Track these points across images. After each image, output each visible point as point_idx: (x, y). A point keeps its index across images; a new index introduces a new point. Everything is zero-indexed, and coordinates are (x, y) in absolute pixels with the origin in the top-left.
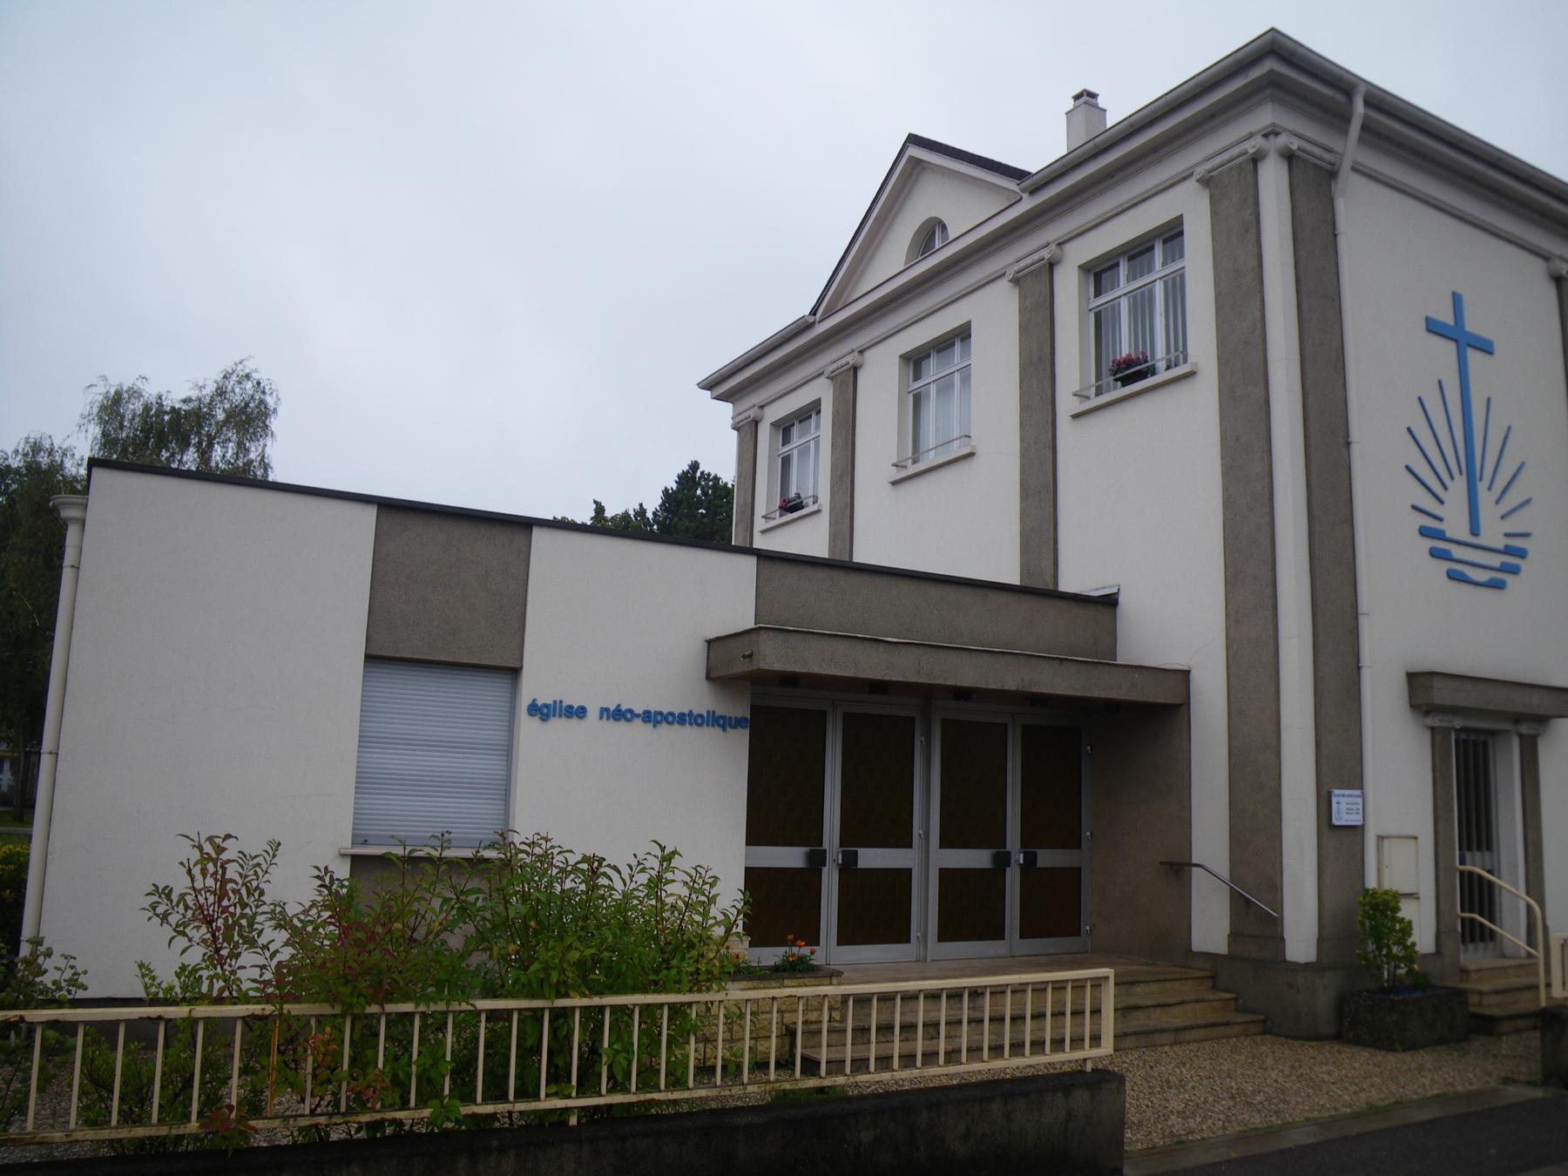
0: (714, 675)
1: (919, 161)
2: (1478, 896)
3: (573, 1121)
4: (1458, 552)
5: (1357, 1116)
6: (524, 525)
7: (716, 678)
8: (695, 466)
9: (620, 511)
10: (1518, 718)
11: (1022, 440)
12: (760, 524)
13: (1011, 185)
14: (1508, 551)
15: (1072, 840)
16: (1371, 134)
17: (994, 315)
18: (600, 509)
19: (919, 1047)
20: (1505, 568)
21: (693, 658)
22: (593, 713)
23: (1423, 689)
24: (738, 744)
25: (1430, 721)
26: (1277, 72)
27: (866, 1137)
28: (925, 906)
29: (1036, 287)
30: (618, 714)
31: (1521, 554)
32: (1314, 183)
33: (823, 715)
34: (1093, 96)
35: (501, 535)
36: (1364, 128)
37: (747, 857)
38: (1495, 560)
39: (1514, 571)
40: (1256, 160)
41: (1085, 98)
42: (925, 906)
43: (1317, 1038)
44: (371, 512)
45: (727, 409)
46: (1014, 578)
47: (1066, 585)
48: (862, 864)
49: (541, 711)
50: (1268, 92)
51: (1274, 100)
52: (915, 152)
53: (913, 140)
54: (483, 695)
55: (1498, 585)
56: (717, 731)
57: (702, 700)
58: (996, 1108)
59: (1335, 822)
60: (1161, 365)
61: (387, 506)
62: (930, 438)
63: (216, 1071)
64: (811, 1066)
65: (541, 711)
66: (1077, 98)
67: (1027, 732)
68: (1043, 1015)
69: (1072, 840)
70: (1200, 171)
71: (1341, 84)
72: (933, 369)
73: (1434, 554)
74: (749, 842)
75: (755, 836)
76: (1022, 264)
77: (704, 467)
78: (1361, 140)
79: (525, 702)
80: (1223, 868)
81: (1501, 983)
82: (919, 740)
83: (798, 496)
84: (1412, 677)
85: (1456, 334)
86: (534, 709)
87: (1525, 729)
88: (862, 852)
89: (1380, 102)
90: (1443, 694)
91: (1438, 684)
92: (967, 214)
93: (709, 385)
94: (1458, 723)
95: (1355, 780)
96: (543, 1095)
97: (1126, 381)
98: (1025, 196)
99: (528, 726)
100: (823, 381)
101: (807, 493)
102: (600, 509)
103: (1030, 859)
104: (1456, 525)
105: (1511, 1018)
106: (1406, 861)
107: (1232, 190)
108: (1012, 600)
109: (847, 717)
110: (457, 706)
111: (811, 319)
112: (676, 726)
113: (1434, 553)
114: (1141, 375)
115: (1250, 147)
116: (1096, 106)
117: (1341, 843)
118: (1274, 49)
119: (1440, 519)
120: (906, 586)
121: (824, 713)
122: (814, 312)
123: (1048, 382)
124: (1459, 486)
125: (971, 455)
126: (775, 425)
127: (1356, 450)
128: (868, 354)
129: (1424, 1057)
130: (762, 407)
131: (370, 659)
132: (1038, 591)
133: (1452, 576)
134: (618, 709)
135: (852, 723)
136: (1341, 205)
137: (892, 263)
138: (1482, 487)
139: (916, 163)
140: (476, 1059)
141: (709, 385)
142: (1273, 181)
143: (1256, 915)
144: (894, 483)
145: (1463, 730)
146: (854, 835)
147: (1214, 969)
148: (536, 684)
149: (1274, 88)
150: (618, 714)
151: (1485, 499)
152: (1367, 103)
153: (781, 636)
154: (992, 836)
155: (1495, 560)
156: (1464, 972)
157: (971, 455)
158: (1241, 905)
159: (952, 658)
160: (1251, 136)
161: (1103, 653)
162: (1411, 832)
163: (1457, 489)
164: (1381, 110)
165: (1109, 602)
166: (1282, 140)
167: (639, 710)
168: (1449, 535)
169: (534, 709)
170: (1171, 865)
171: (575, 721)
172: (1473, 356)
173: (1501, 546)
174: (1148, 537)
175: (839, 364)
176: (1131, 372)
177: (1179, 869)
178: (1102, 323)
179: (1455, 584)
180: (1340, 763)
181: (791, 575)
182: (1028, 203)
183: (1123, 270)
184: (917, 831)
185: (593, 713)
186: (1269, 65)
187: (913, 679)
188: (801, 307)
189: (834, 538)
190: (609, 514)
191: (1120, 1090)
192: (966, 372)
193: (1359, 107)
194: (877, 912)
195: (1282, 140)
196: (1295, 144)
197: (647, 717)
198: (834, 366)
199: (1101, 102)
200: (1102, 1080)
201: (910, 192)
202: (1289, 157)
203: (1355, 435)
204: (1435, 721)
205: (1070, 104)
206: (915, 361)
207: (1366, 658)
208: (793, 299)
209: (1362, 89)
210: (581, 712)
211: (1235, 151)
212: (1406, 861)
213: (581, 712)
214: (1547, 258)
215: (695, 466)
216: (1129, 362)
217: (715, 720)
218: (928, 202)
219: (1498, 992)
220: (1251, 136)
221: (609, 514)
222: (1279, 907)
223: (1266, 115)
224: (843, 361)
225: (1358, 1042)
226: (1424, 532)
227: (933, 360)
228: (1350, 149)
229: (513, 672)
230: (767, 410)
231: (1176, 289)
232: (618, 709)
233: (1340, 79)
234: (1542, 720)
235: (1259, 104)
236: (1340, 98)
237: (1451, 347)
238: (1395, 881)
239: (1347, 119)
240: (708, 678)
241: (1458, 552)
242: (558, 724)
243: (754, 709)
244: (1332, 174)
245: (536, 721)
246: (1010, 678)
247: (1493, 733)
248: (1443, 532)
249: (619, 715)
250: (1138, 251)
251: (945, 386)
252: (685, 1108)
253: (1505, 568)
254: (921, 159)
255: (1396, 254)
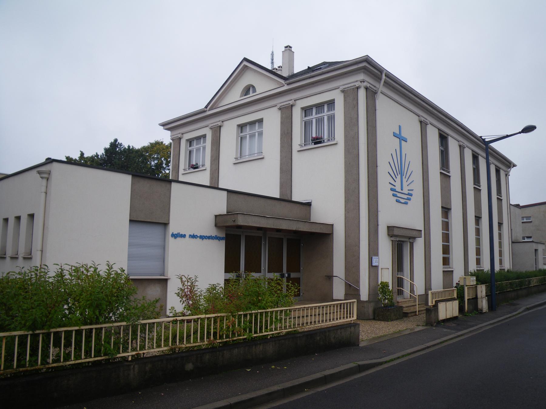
0: (219, 225)
1: (247, 66)
2: (400, 282)
3: (130, 359)
4: (399, 195)
5: (392, 334)
7: (217, 226)
8: (116, 140)
9: (90, 155)
10: (410, 238)
11: (281, 156)
12: (181, 171)
13: (282, 81)
15: (298, 271)
16: (386, 84)
17: (272, 119)
18: (82, 154)
19: (279, 325)
21: (211, 221)
22: (187, 236)
23: (390, 229)
24: (223, 243)
25: (392, 239)
26: (367, 66)
27: (318, 338)
29: (287, 112)
30: (193, 236)
31: (411, 195)
32: (371, 94)
34: (291, 47)
36: (385, 82)
37: (225, 276)
38: (406, 197)
39: (409, 199)
40: (358, 88)
41: (288, 48)
43: (370, 320)
45: (169, 132)
46: (278, 196)
47: (294, 199)
48: (291, 277)
49: (175, 236)
50: (363, 70)
51: (364, 73)
52: (245, 63)
53: (245, 59)
54: (157, 231)
55: (406, 203)
57: (213, 232)
58: (339, 331)
60: (326, 141)
62: (247, 151)
63: (209, 326)
64: (285, 327)
65: (175, 236)
66: (286, 47)
67: (288, 240)
68: (295, 318)
69: (298, 271)
71: (380, 70)
72: (248, 131)
73: (394, 195)
74: (225, 272)
75: (226, 271)
76: (282, 104)
77: (119, 141)
78: (384, 85)
80: (343, 276)
81: (407, 305)
82: (263, 242)
83: (197, 164)
84: (388, 227)
85: (399, 136)
87: (411, 241)
88: (291, 274)
89: (389, 76)
90: (396, 232)
91: (395, 229)
92: (264, 86)
93: (163, 125)
94: (398, 239)
95: (377, 254)
96: (147, 348)
97: (315, 143)
98: (286, 85)
99: (171, 242)
100: (208, 128)
101: (200, 163)
102: (82, 154)
103: (289, 275)
104: (398, 188)
105: (411, 313)
106: (386, 276)
107: (350, 95)
108: (276, 202)
109: (246, 236)
110: (151, 234)
111: (206, 109)
114: (320, 142)
115: (357, 84)
116: (291, 51)
117: (373, 269)
118: (367, 60)
120: (262, 200)
121: (240, 235)
122: (206, 107)
123: (290, 140)
124: (399, 177)
125: (263, 158)
126: (187, 140)
127: (378, 168)
128: (224, 123)
129: (395, 323)
130: (182, 134)
131: (131, 221)
132: (285, 199)
133: (397, 201)
134: (193, 235)
136: (378, 102)
137: (235, 97)
138: (404, 177)
139: (246, 66)
140: (38, 349)
141: (163, 125)
142: (362, 94)
143: (352, 290)
144: (234, 164)
145: (399, 241)
148: (173, 228)
149: (365, 70)
150: (193, 236)
151: (404, 180)
152: (385, 75)
153: (243, 216)
154: (279, 269)
156: (398, 302)
157: (263, 158)
158: (348, 286)
159: (281, 221)
160: (357, 81)
161: (307, 219)
163: (398, 179)
165: (309, 204)
166: (365, 84)
170: (328, 276)
172: (403, 142)
174: (321, 186)
175: (215, 124)
176: (317, 141)
177: (330, 277)
178: (307, 125)
180: (373, 251)
181: (235, 196)
182: (286, 88)
183: (314, 110)
184: (262, 268)
185: (187, 236)
186: (365, 64)
187: (272, 227)
188: (202, 106)
189: (211, 178)
190: (85, 156)
191: (359, 327)
192: (261, 134)
193: (384, 77)
195: (365, 84)
196: (368, 85)
198: (213, 125)
199: (293, 49)
200: (354, 325)
201: (242, 75)
202: (367, 88)
203: (378, 165)
204: (393, 239)
205: (283, 49)
206: (241, 127)
207: (380, 223)
208: (198, 102)
209: (385, 72)
210: (184, 236)
211: (352, 84)
212: (386, 276)
215: (116, 140)
216: (317, 138)
217: (216, 238)
218: (248, 79)
219: (407, 307)
220: (357, 81)
221: (85, 156)
222: (359, 286)
223: (361, 76)
224: (216, 124)
225: (379, 320)
226: (392, 189)
227: (248, 127)
228: (381, 87)
229: (166, 225)
230: (184, 135)
231: (331, 119)
232: (193, 235)
233: (380, 69)
234: (414, 238)
235: (360, 73)
236: (379, 73)
237: (398, 140)
238: (385, 280)
239: (381, 80)
240: (216, 226)
241: (399, 195)
242: (179, 239)
243: (226, 234)
244: (375, 93)
245: (173, 238)
246: (284, 225)
247: (403, 241)
250: (319, 107)
251: (252, 136)
252: (195, 349)
254: (247, 65)
255: (391, 116)
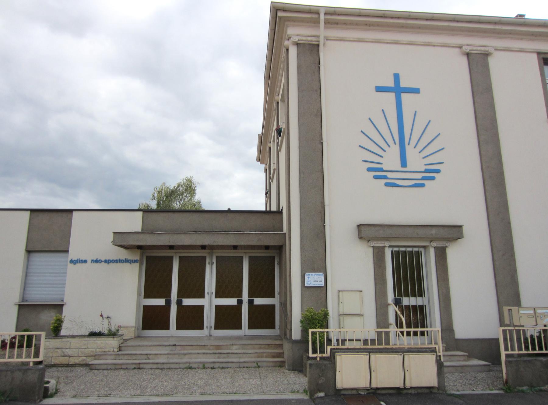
6: (71, 211)
14: (426, 171)
20: (424, 178)
23: (365, 232)
28: (209, 317)
33: (242, 257)
35: (65, 215)
42: (209, 317)
44: (29, 213)
49: (73, 262)
56: (128, 264)
59: (306, 285)
61: (32, 211)
70: (468, 49)
79: (69, 259)
86: (72, 262)
90: (366, 232)
99: (70, 266)
112: (115, 263)
113: (376, 177)
119: (381, 164)
121: (205, 257)
124: (396, 149)
135: (182, 260)
146: (182, 294)
147: (296, 342)
148: (73, 254)
155: (419, 176)
162: (360, 289)
164: (331, 14)
167: (103, 260)
168: (384, 169)
169: (72, 262)
171: (84, 264)
173: (423, 170)
179: (390, 188)
194: (191, 319)
197: (107, 262)
202: (297, 44)
210: (85, 261)
213: (85, 261)
214: (460, 47)
242: (78, 265)
245: (72, 265)
248: (382, 168)
249: (97, 261)
253: (424, 178)
